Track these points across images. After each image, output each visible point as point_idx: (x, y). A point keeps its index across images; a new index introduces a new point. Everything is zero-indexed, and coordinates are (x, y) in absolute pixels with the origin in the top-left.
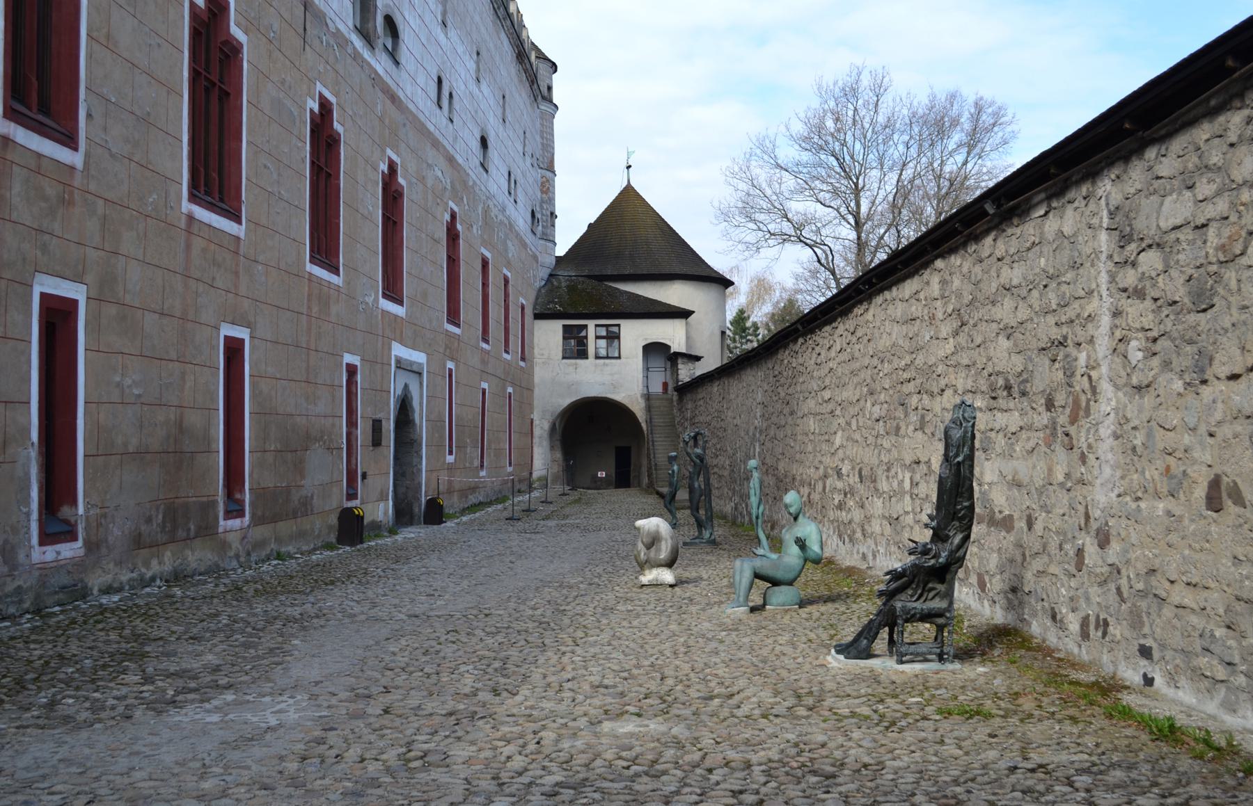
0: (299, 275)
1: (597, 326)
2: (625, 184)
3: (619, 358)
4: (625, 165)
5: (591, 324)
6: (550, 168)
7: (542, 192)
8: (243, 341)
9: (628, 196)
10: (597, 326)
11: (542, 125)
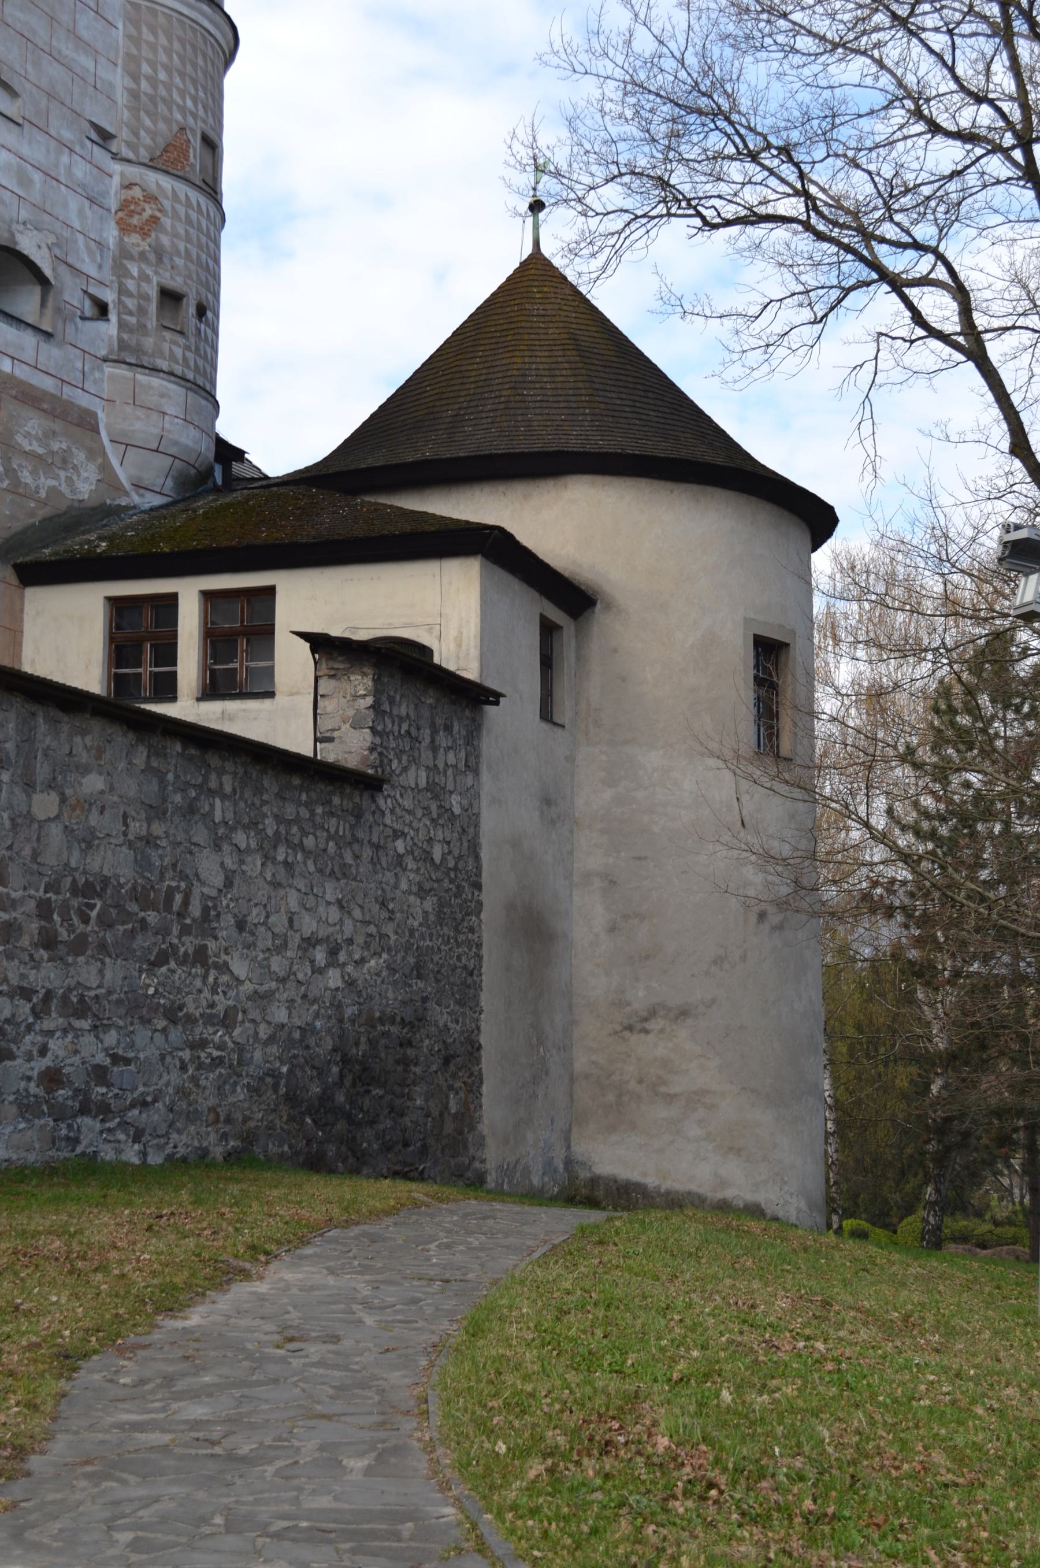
2: (528, 250)
3: (271, 695)
5: (189, 594)
7: (124, 228)
8: (174, 699)
11: (135, 40)
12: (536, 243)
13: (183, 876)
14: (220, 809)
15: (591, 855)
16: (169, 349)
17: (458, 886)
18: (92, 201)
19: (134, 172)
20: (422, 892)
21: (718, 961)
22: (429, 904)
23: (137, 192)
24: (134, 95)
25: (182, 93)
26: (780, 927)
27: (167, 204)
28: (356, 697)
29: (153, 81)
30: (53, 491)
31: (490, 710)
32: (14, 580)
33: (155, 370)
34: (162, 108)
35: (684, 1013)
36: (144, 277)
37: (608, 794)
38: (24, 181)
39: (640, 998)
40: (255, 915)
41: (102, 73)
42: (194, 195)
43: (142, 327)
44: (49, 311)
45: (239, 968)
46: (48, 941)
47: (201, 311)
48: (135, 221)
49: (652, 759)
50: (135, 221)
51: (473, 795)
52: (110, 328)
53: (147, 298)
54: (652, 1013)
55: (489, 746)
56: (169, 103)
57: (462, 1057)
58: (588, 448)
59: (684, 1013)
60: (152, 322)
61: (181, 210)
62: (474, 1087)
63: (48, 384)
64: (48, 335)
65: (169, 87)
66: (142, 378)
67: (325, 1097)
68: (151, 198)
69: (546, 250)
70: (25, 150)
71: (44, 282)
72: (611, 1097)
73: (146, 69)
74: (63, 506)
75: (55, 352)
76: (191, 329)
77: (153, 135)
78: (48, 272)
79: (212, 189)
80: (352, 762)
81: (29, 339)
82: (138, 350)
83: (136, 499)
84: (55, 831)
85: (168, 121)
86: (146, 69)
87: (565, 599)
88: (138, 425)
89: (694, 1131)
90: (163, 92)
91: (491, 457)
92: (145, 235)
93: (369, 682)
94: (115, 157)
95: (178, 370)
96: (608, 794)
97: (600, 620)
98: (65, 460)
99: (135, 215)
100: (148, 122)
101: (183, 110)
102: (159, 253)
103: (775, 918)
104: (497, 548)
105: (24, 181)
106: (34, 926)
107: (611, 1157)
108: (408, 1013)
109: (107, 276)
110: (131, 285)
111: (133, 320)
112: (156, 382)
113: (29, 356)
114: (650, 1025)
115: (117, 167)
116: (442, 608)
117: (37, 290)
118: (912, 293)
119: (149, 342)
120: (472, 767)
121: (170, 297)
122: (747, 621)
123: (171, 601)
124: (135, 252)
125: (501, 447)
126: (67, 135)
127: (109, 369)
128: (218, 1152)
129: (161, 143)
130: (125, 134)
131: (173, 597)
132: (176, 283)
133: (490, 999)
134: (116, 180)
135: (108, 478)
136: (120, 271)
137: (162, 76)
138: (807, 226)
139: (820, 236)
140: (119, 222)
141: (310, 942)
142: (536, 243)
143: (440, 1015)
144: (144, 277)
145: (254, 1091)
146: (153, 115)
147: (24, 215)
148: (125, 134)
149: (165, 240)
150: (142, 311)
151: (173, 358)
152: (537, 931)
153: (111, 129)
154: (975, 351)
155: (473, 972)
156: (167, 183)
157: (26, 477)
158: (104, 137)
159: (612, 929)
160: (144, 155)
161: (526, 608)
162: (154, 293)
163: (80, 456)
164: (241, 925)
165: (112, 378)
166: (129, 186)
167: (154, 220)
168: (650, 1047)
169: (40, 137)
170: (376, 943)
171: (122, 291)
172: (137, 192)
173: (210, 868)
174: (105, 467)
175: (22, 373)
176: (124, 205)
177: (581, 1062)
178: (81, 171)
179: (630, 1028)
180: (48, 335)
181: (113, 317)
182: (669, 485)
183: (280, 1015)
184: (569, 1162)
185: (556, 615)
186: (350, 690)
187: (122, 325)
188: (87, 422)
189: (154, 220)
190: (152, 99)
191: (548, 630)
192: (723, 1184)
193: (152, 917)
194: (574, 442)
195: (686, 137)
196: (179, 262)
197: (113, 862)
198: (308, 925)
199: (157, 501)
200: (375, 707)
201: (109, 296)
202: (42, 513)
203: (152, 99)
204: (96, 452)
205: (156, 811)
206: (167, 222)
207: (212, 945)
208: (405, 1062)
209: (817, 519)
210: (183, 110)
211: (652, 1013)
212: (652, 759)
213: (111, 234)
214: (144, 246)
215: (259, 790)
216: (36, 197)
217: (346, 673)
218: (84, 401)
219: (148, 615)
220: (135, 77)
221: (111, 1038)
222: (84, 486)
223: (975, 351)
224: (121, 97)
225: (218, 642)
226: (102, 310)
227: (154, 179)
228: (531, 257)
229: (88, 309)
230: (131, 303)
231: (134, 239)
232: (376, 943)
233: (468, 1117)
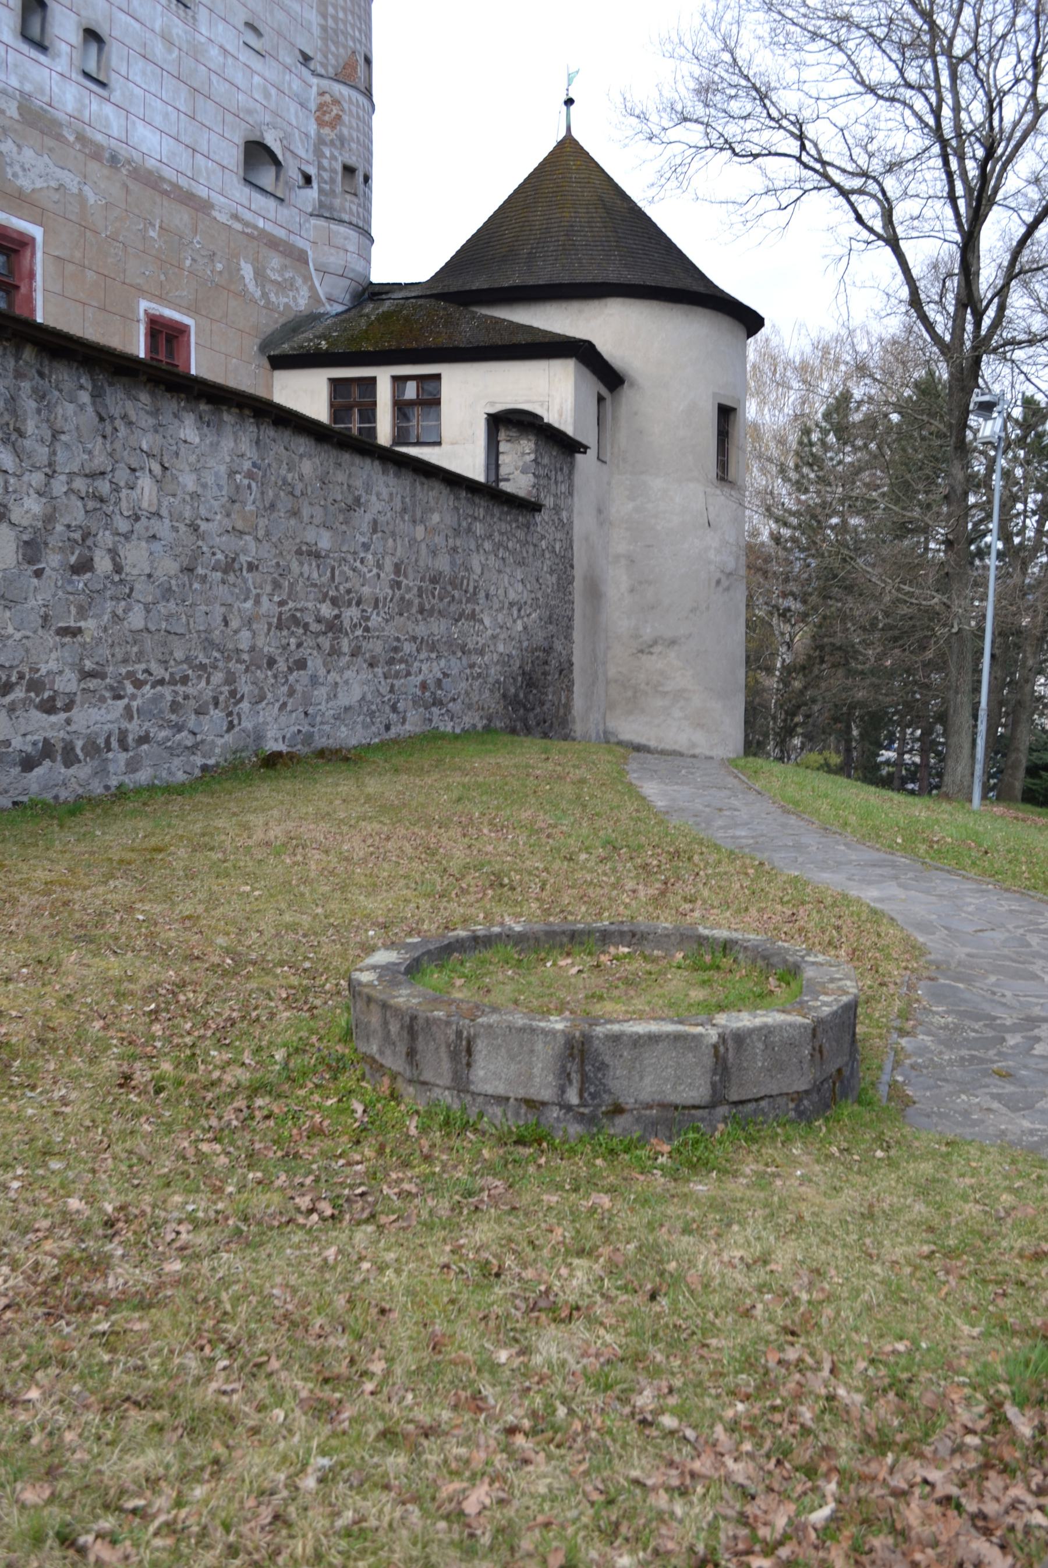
0: (192, 309)
1: (395, 379)
2: (562, 133)
4: (564, 98)
5: (384, 377)
6: (356, 72)
7: (321, 123)
9: (568, 156)
10: (395, 379)
12: (569, 129)
13: (467, 570)
14: (479, 528)
15: (620, 545)
16: (347, 206)
17: (564, 564)
18: (302, 105)
19: (325, 83)
20: (552, 572)
21: (693, 610)
22: (554, 579)
23: (327, 98)
24: (324, 28)
25: (353, 26)
26: (728, 589)
27: (346, 106)
28: (523, 454)
29: (336, 19)
30: (287, 306)
31: (579, 457)
32: (267, 365)
33: (341, 221)
34: (341, 38)
35: (673, 642)
36: (333, 158)
37: (630, 506)
38: (267, 96)
39: (648, 632)
40: (492, 591)
41: (306, 15)
42: (355, 95)
43: (333, 191)
44: (281, 184)
45: (487, 621)
46: (421, 611)
47: (367, 179)
48: (327, 118)
49: (657, 483)
50: (327, 118)
51: (570, 509)
52: (312, 194)
53: (333, 171)
54: (655, 642)
55: (578, 478)
56: (345, 33)
57: (566, 669)
58: (622, 281)
59: (673, 642)
60: (339, 189)
61: (354, 109)
62: (570, 690)
63: (281, 233)
64: (282, 200)
65: (345, 22)
66: (334, 227)
67: (516, 695)
68: (336, 102)
69: (575, 134)
70: (267, 74)
71: (277, 163)
72: (630, 694)
73: (331, 10)
74: (292, 316)
75: (286, 212)
76: (360, 193)
77: (336, 57)
78: (280, 157)
79: (368, 93)
80: (522, 494)
81: (272, 203)
82: (331, 208)
83: (328, 308)
84: (423, 546)
85: (345, 47)
86: (331, 10)
87: (606, 376)
88: (332, 259)
89: (677, 713)
90: (341, 26)
91: (561, 285)
92: (333, 128)
93: (532, 445)
94: (314, 73)
95: (354, 220)
96: (630, 506)
97: (626, 392)
98: (291, 285)
99: (327, 115)
100: (333, 48)
101: (354, 39)
102: (342, 139)
103: (725, 583)
104: (584, 353)
105: (267, 96)
106: (416, 601)
107: (630, 729)
108: (546, 645)
109: (311, 157)
110: (325, 163)
111: (327, 187)
112: (342, 229)
113: (271, 215)
114: (655, 650)
115: (315, 81)
116: (551, 391)
117: (273, 170)
118: (853, 198)
119: (337, 202)
120: (571, 494)
121: (349, 170)
122: (715, 395)
123: (371, 383)
124: (328, 139)
125: (566, 278)
126: (288, 61)
127: (313, 221)
128: (480, 726)
129: (342, 63)
130: (319, 57)
131: (373, 380)
132: (352, 161)
133: (577, 635)
134: (315, 89)
135: (314, 296)
136: (319, 153)
137: (341, 15)
138: (799, 159)
139: (806, 166)
140: (317, 119)
141: (511, 604)
142: (569, 129)
143: (558, 646)
144: (333, 158)
145: (491, 691)
146: (336, 44)
147: (268, 119)
148: (319, 57)
149: (345, 131)
150: (333, 181)
151: (351, 213)
152: (595, 593)
153: (311, 54)
154: (893, 242)
155: (570, 619)
156: (345, 91)
157: (273, 297)
158: (306, 59)
159: (632, 590)
160: (331, 72)
161: (593, 386)
162: (339, 168)
163: (299, 281)
164: (487, 596)
165: (315, 227)
166: (322, 94)
167: (338, 117)
168: (653, 663)
169: (274, 64)
170: (535, 604)
171: (320, 167)
172: (327, 98)
173: (476, 562)
174: (312, 288)
175: (269, 227)
176: (321, 107)
177: (612, 672)
178: (296, 85)
179: (642, 651)
180: (282, 200)
181: (315, 184)
182: (671, 305)
183: (501, 648)
184: (605, 732)
185: (605, 392)
186: (520, 449)
187: (321, 191)
188: (300, 258)
189: (338, 117)
190: (335, 31)
191: (601, 399)
192: (694, 745)
193: (456, 593)
194: (612, 275)
195: (728, 100)
196: (354, 146)
197: (443, 564)
198: (512, 596)
199: (340, 308)
200: (535, 460)
201: (312, 171)
202: (282, 320)
203: (335, 31)
204: (307, 278)
205: (457, 532)
206: (346, 118)
207: (478, 609)
208: (545, 674)
209: (750, 321)
210: (354, 39)
211: (655, 642)
212: (657, 483)
213: (312, 128)
214: (333, 136)
215: (493, 516)
216: (273, 106)
217: (518, 439)
218: (301, 243)
219: (355, 391)
220: (324, 16)
221: (443, 662)
222: (301, 302)
223: (893, 242)
224: (316, 31)
225: (401, 407)
226: (308, 180)
227: (338, 89)
228: (561, 145)
229: (301, 181)
230: (326, 175)
231: (326, 131)
232: (535, 604)
233: (568, 706)
